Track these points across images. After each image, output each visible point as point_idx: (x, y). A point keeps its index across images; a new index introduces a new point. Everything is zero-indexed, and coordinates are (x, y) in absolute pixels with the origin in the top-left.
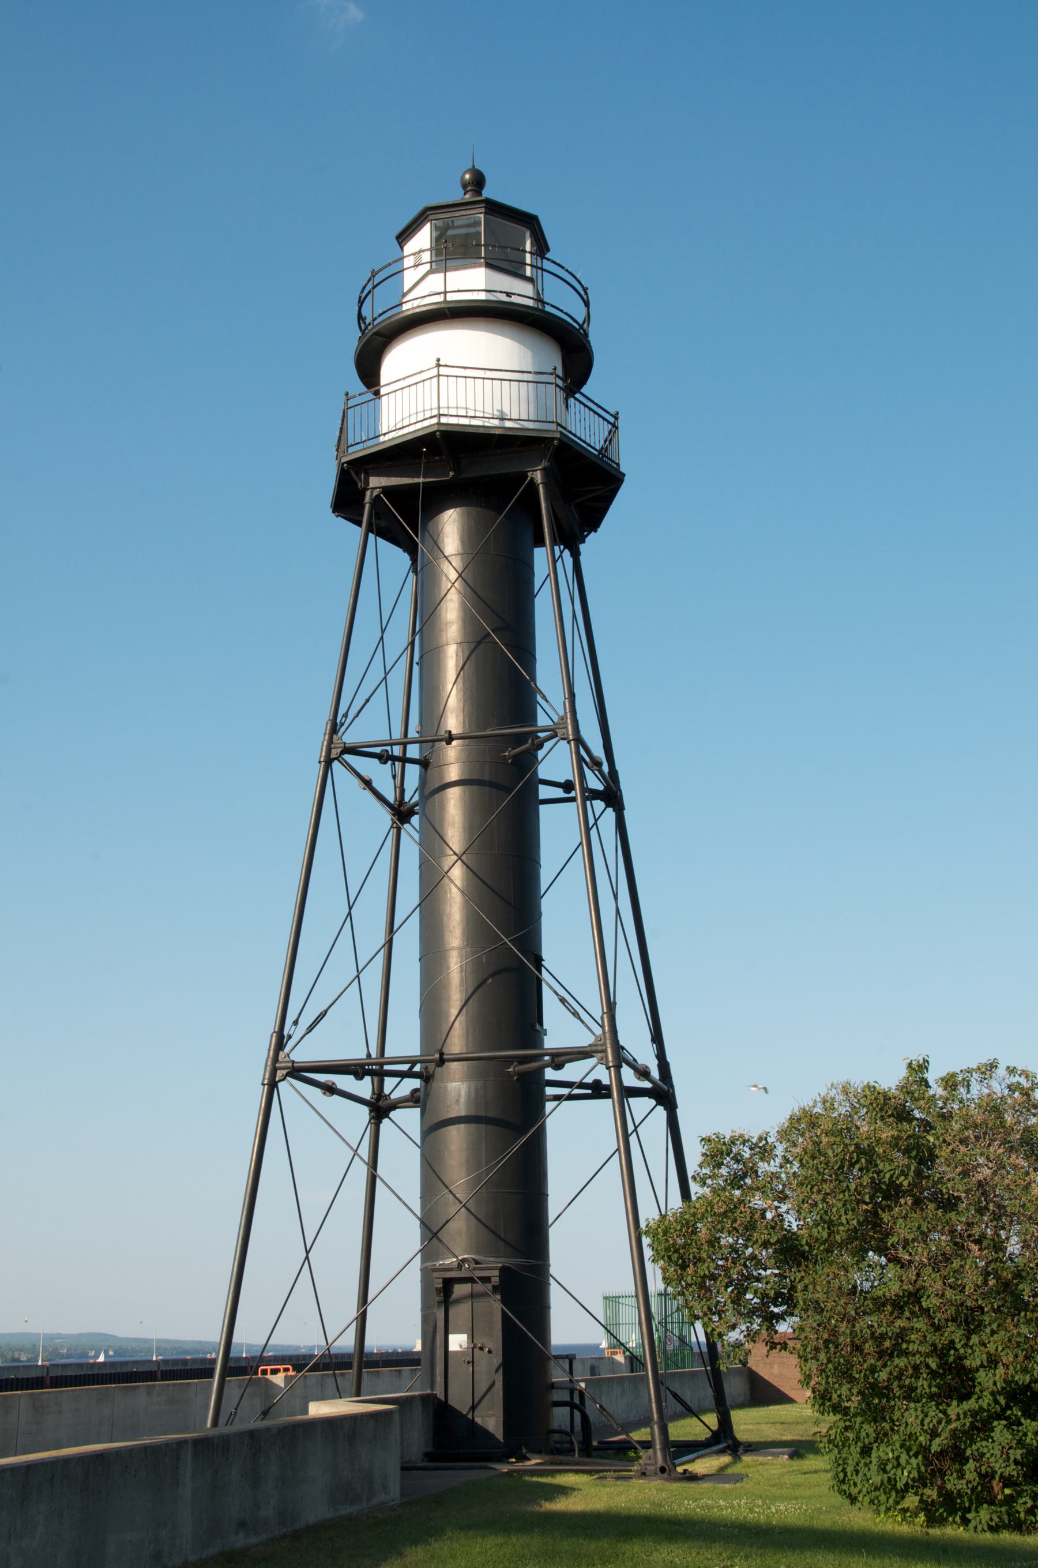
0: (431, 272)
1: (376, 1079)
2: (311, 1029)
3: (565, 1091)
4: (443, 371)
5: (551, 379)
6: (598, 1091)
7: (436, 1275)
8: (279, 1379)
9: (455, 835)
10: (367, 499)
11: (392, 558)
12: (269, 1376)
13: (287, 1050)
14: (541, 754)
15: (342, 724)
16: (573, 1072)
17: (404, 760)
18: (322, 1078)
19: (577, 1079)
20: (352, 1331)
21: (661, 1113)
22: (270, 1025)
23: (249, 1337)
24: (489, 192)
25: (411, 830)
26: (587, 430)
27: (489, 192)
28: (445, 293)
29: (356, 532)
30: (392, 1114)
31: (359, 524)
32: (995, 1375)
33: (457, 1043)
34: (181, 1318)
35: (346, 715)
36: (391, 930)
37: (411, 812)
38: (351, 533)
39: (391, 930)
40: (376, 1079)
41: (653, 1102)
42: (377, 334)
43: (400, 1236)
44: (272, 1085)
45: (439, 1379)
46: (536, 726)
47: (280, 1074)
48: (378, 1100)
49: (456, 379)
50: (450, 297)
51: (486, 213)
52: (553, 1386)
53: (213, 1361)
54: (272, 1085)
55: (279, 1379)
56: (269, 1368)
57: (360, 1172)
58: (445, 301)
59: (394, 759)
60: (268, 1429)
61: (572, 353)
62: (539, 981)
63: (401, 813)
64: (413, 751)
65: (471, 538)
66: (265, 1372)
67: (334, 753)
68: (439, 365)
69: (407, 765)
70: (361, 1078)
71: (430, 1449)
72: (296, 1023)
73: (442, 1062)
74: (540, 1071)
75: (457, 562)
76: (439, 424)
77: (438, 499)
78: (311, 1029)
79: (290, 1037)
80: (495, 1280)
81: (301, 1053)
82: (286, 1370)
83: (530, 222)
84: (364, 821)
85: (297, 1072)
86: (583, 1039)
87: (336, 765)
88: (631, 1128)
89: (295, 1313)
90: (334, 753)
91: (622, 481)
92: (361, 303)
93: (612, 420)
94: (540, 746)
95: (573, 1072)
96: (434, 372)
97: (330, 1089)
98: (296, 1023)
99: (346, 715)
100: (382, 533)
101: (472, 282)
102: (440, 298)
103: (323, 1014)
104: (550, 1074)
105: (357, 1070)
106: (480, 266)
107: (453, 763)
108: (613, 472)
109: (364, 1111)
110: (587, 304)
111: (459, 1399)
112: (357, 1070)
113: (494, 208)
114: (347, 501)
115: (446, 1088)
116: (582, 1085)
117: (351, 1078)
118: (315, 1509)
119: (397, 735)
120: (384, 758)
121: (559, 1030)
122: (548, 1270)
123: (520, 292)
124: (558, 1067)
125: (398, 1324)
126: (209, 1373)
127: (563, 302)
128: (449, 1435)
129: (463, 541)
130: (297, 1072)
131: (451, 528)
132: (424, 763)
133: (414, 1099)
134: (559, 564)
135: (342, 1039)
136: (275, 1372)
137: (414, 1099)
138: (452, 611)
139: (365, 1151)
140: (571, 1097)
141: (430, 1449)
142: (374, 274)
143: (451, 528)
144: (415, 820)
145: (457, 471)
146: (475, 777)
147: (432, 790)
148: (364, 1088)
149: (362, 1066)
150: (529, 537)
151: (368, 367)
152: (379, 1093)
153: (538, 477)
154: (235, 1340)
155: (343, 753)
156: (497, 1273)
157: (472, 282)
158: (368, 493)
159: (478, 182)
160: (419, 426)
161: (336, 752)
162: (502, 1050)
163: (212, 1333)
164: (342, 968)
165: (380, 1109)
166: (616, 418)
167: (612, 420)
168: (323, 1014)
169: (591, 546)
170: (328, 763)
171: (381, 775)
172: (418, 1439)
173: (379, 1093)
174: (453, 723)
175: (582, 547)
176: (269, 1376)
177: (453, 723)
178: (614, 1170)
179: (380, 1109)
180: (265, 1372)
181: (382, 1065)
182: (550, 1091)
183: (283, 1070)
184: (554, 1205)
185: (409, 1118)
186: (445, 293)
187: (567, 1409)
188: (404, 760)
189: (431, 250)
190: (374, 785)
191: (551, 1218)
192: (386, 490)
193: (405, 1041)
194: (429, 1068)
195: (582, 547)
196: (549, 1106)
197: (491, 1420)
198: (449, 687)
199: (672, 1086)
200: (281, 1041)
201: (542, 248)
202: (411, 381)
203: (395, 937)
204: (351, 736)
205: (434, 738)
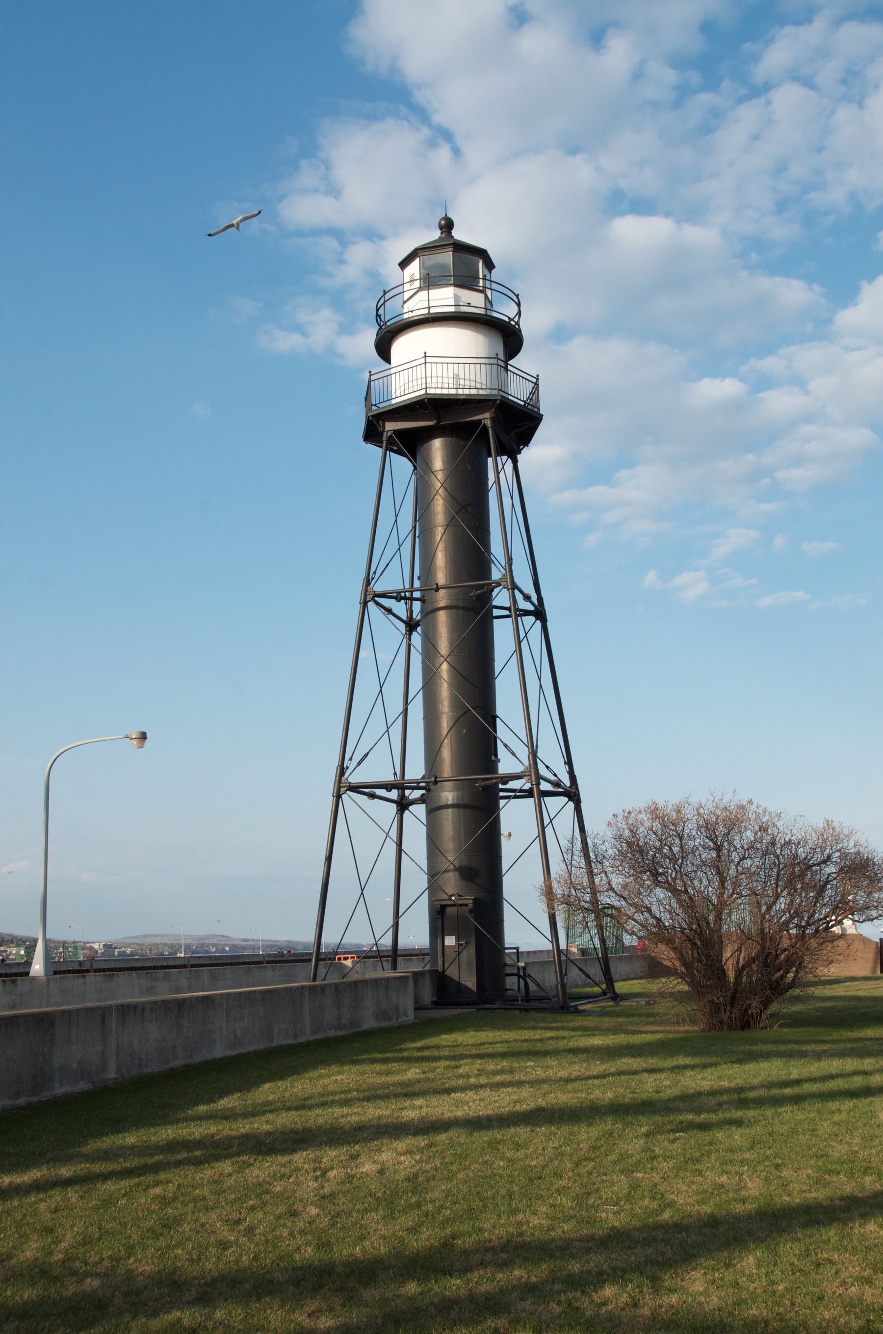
0: (420, 289)
1: (390, 953)
2: (359, 764)
3: (513, 794)
4: (428, 360)
5: (495, 361)
6: (529, 794)
7: (436, 903)
8: (349, 963)
9: (444, 646)
10: (384, 438)
11: (401, 465)
12: (342, 961)
13: (346, 776)
14: (494, 594)
15: (373, 579)
16: (513, 785)
17: (412, 599)
18: (367, 790)
19: (518, 787)
20: (390, 934)
21: (571, 805)
22: (336, 762)
23: (330, 938)
24: (458, 234)
25: (417, 638)
26: (518, 392)
27: (458, 234)
28: (429, 308)
29: (378, 451)
30: (410, 808)
31: (381, 447)
32: (674, 1007)
33: (447, 769)
34: (289, 926)
35: (375, 573)
36: (406, 703)
37: (417, 624)
38: (376, 452)
39: (406, 703)
40: (390, 953)
41: (566, 799)
42: (388, 332)
43: (416, 881)
44: (338, 797)
45: (440, 962)
46: (490, 579)
47: (342, 790)
48: (401, 799)
49: (439, 362)
50: (432, 311)
51: (453, 251)
52: (506, 965)
53: (311, 954)
54: (338, 797)
55: (349, 963)
56: (342, 956)
57: (391, 848)
58: (426, 394)
59: (405, 598)
60: (344, 983)
61: (510, 338)
62: (495, 738)
63: (411, 626)
64: (417, 595)
65: (451, 457)
66: (340, 959)
67: (369, 597)
68: (425, 357)
69: (414, 602)
70: (399, 601)
71: (435, 999)
72: (351, 759)
73: (436, 782)
74: (496, 784)
75: (440, 476)
76: (426, 394)
77: (427, 435)
78: (359, 764)
79: (347, 768)
80: (471, 906)
81: (355, 778)
82: (353, 958)
83: (482, 254)
84: (386, 632)
85: (355, 788)
86: (518, 769)
87: (371, 605)
88: (546, 820)
89: (358, 927)
90: (369, 597)
91: (541, 419)
92: (377, 310)
93: (534, 380)
94: (493, 590)
95: (513, 785)
96: (423, 361)
97: (372, 796)
98: (351, 759)
99: (375, 573)
100: (392, 450)
101: (444, 298)
102: (426, 311)
103: (366, 755)
104: (501, 786)
105: (388, 787)
106: (449, 285)
107: (442, 598)
108: (536, 415)
109: (394, 807)
110: (519, 305)
111: (452, 972)
112: (388, 787)
113: (461, 248)
114: (372, 433)
115: (440, 797)
116: (521, 791)
117: (384, 790)
118: (369, 1023)
119: (407, 586)
120: (398, 599)
121: (506, 764)
122: (502, 896)
123: (474, 301)
124: (505, 783)
125: (416, 933)
126: (310, 960)
127: (505, 311)
128: (445, 992)
129: (443, 462)
130: (355, 788)
131: (437, 448)
132: (422, 600)
133: (422, 800)
134: (502, 475)
135: (378, 769)
136: (346, 959)
137: (422, 800)
138: (439, 506)
139: (394, 834)
140: (516, 797)
141: (435, 999)
142: (385, 293)
143: (437, 448)
144: (419, 629)
145: (439, 421)
146: (454, 604)
147: (429, 612)
148: (394, 794)
149: (399, 593)
150: (485, 452)
151: (383, 349)
152: (402, 796)
153: (488, 423)
154: (323, 941)
155: (373, 597)
156: (471, 901)
157: (444, 298)
158: (385, 434)
159: (447, 226)
160: (413, 395)
161: (369, 597)
162: (471, 775)
163: (310, 937)
164: (377, 726)
165: (403, 805)
166: (538, 379)
167: (534, 380)
168: (366, 755)
169: (526, 456)
170: (365, 604)
171: (400, 608)
172: (428, 995)
173: (402, 796)
174: (441, 578)
175: (518, 456)
176: (342, 961)
177: (441, 578)
178: (537, 846)
179: (403, 805)
180: (340, 959)
181: (412, 592)
182: (501, 794)
183: (343, 787)
184: (505, 864)
185: (420, 810)
186: (429, 308)
187: (516, 978)
188: (412, 599)
189: (420, 279)
190: (394, 611)
191: (504, 869)
192: (396, 432)
193: (416, 770)
194: (431, 782)
195: (518, 456)
196: (502, 802)
197: (470, 982)
198: (438, 538)
199: (578, 789)
200: (342, 770)
201: (490, 265)
202: (410, 365)
203: (409, 707)
204: (378, 587)
205: (430, 588)
